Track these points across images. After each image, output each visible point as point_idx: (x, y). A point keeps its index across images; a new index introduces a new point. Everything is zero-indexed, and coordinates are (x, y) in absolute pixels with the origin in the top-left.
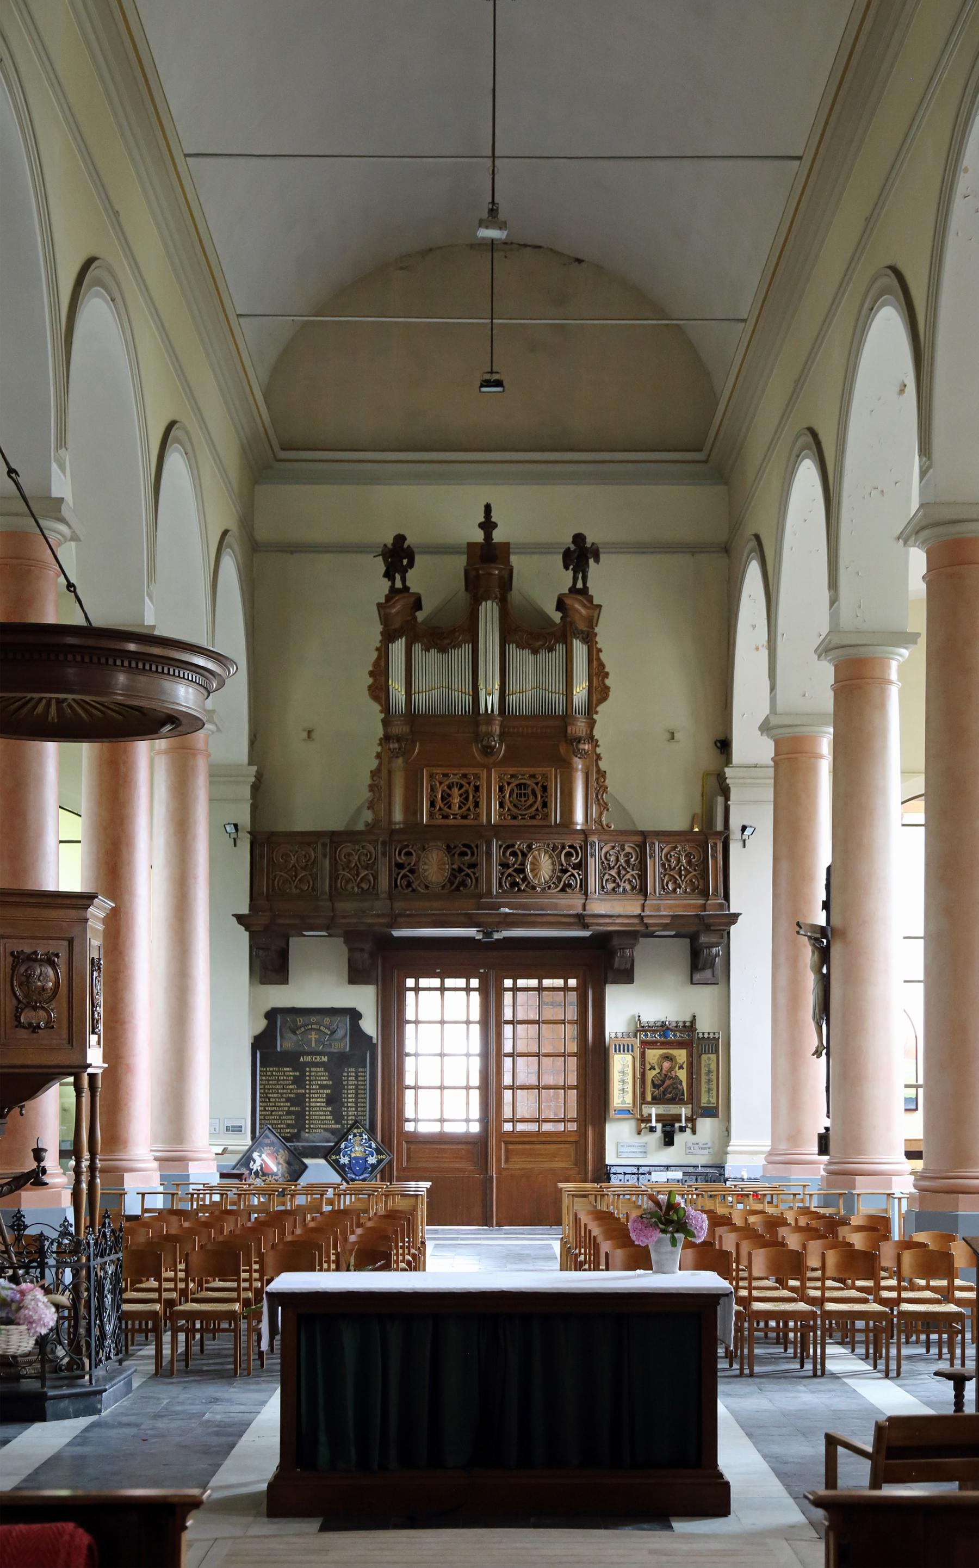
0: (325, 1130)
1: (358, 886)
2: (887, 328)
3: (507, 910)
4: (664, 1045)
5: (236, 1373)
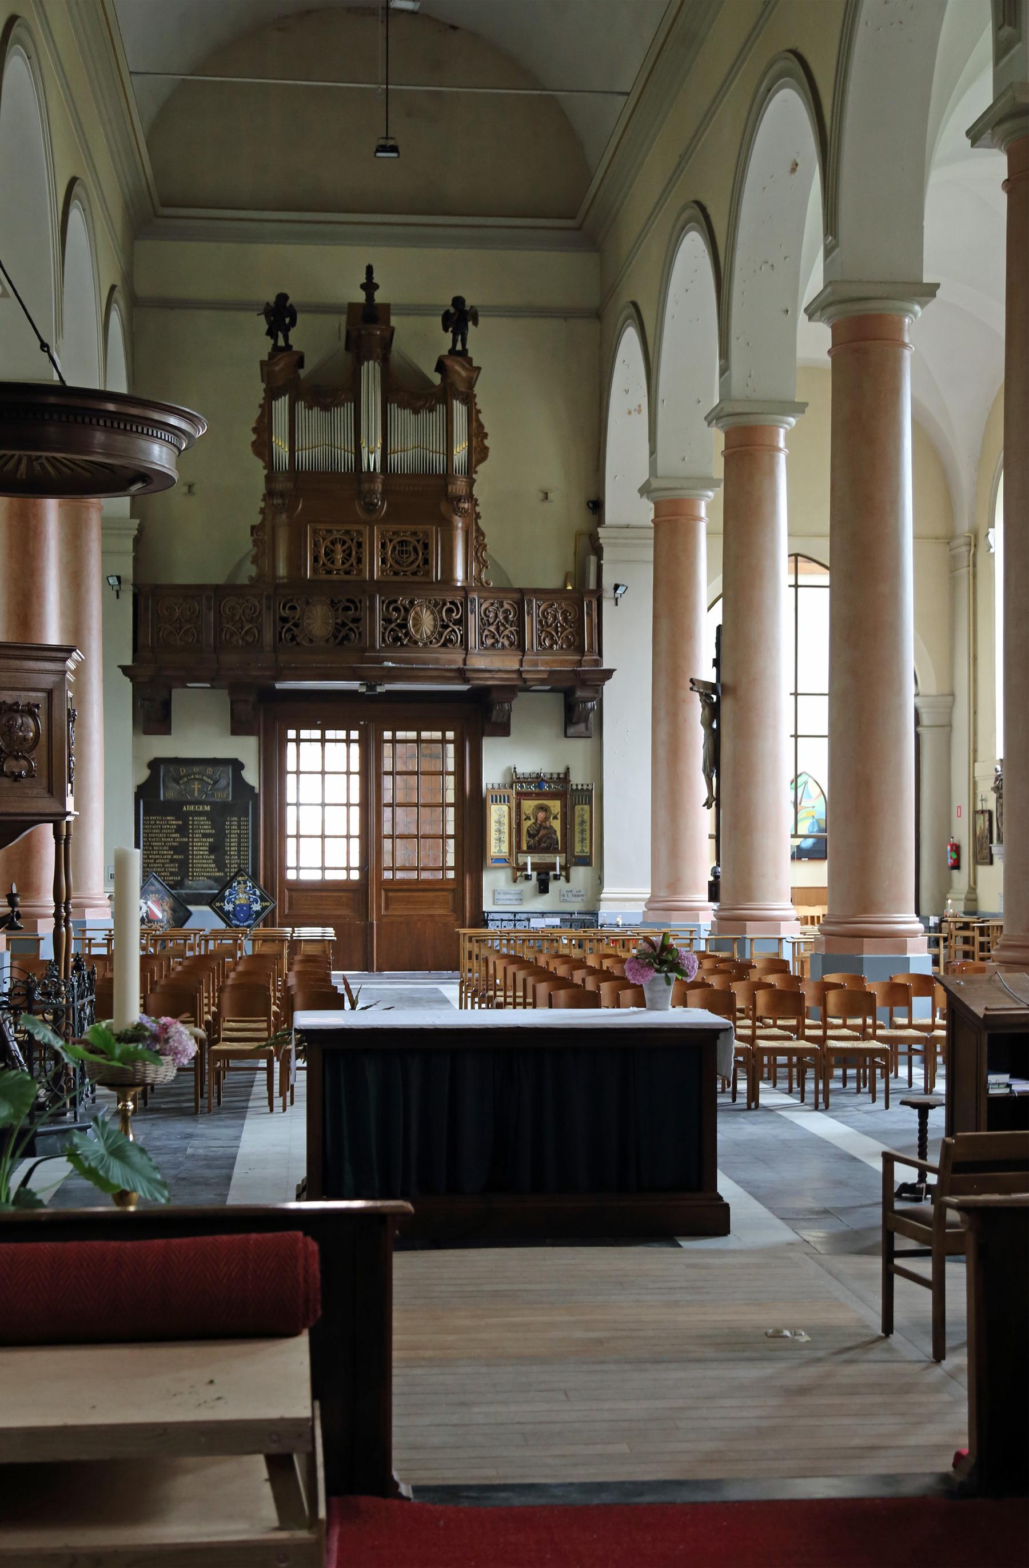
0: (209, 877)
1: (243, 639)
2: (787, 111)
3: (390, 664)
4: (539, 796)
5: (197, 1111)
